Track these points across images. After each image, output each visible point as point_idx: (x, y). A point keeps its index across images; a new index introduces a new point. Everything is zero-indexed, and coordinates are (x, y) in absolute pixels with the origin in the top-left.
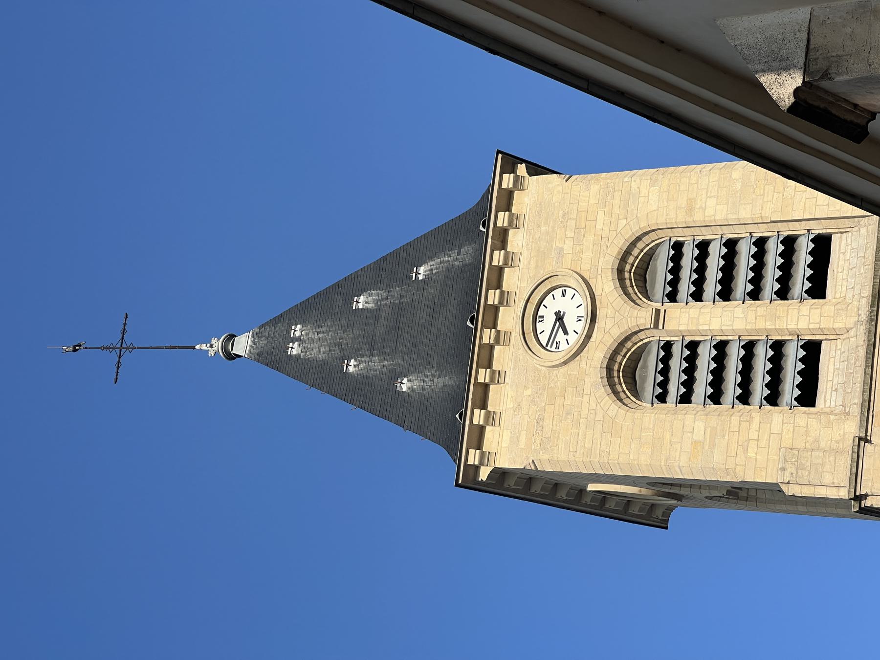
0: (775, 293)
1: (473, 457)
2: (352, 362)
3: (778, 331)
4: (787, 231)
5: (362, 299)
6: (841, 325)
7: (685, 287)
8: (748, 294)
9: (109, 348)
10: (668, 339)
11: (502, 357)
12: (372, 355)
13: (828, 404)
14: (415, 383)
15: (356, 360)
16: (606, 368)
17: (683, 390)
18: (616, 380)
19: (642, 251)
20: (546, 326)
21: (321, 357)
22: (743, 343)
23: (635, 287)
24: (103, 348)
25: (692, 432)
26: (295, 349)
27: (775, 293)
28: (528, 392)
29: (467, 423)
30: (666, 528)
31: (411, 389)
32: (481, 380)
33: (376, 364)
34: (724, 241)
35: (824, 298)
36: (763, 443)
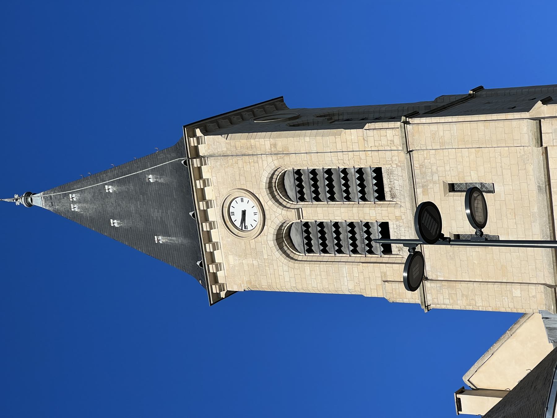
1: (215, 289)
10: (306, 221)
11: (215, 236)
16: (280, 249)
18: (274, 188)
19: (277, 179)
20: (237, 219)
23: (290, 248)
29: (198, 211)
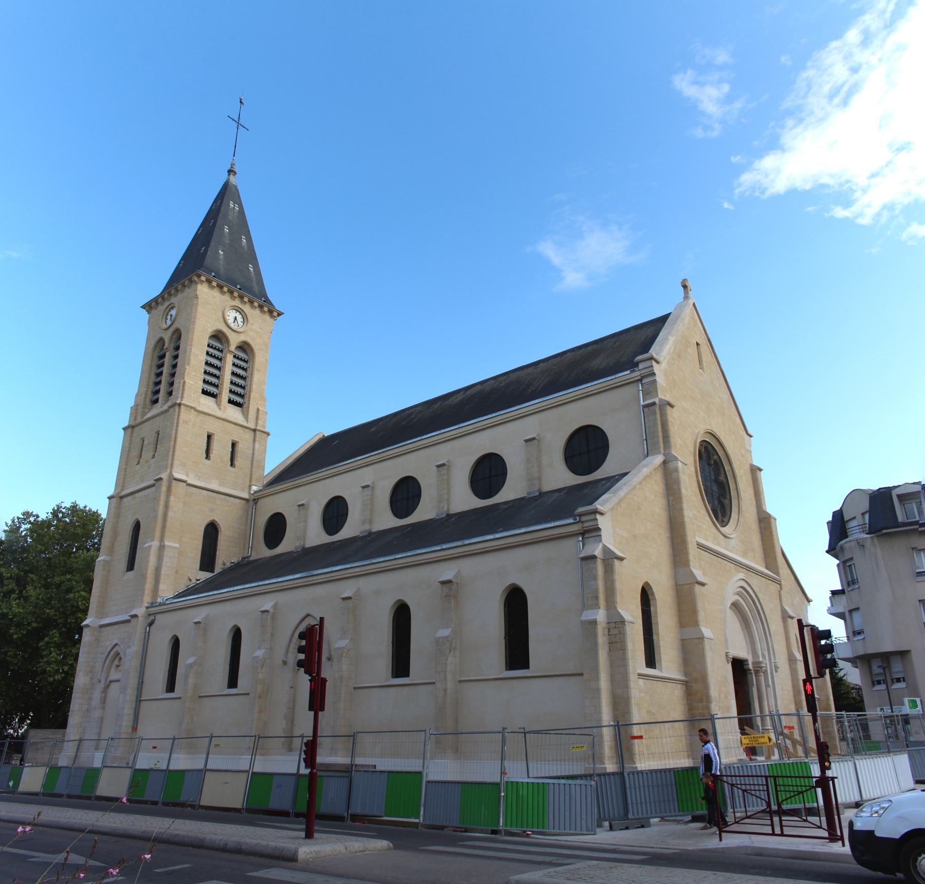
1: (203, 278)
2: (228, 231)
5: (245, 241)
24: (239, 115)
26: (232, 206)
28: (218, 303)
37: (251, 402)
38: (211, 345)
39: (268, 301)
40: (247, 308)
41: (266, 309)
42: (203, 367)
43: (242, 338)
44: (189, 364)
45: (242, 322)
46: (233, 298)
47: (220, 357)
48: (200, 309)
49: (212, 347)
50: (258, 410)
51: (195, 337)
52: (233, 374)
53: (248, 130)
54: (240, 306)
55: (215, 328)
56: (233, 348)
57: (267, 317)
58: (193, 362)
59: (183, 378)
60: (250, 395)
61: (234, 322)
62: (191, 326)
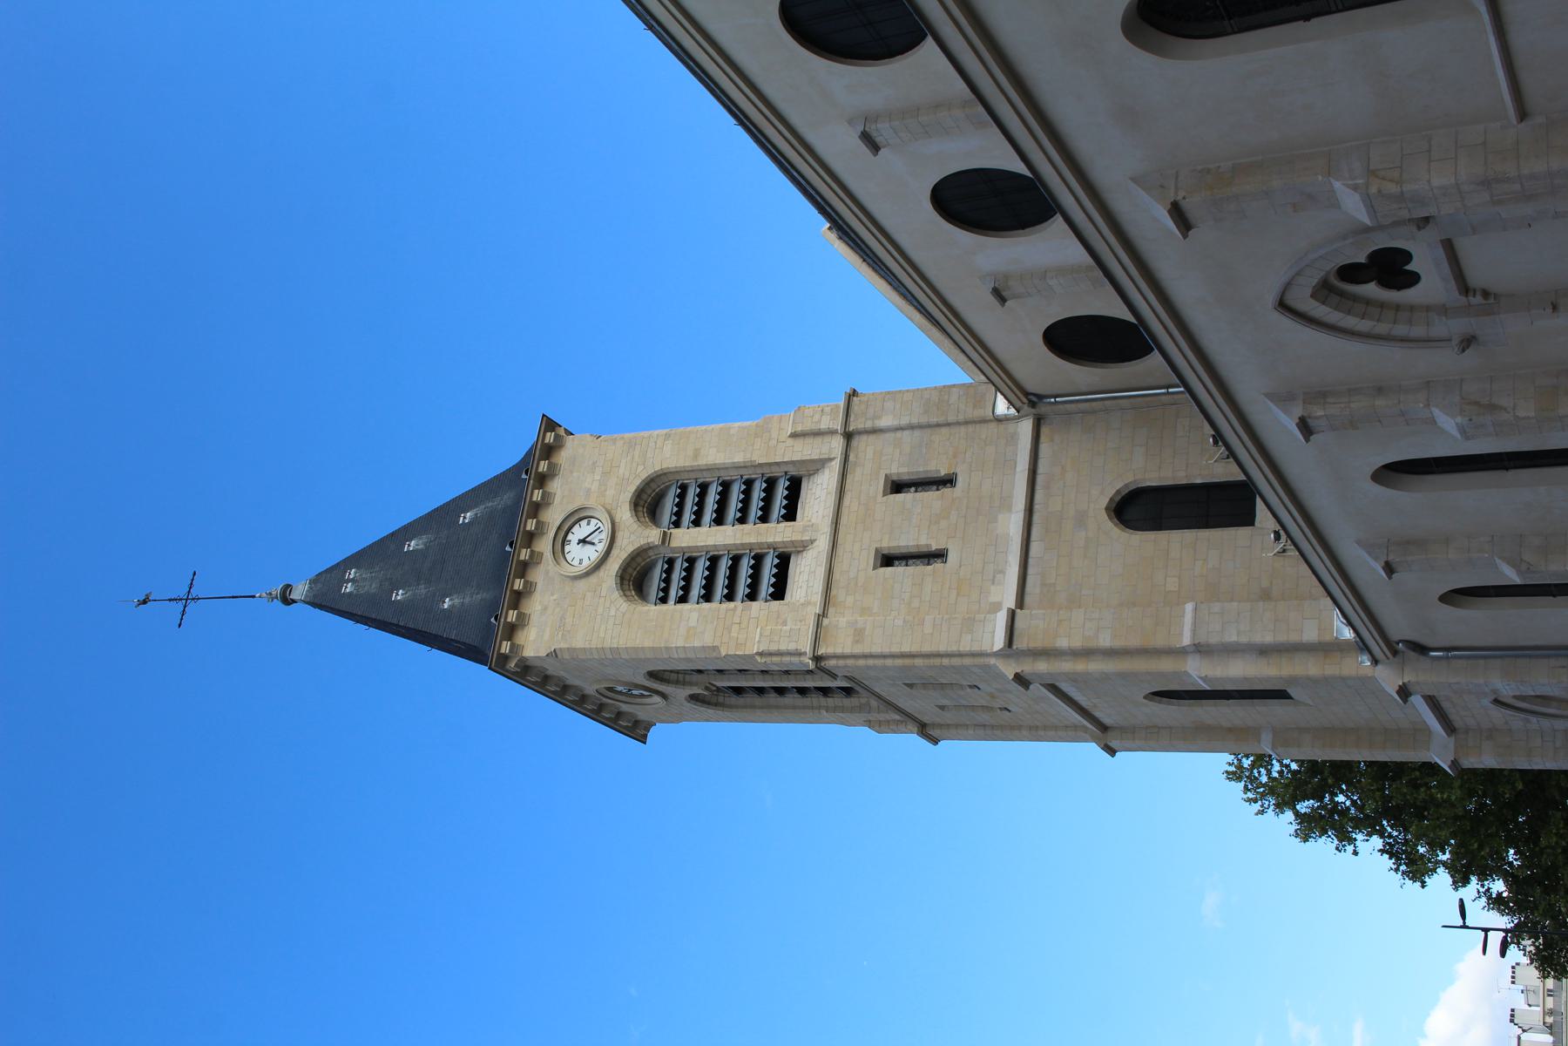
0: (770, 595)
1: (505, 647)
3: (760, 545)
4: (769, 473)
6: (808, 538)
7: (688, 516)
8: (737, 520)
9: (176, 600)
10: (671, 555)
12: (418, 585)
13: (794, 599)
14: (456, 601)
15: (403, 590)
17: (681, 593)
21: (373, 590)
22: (731, 556)
24: (170, 600)
25: (688, 621)
26: (349, 588)
27: (770, 595)
28: (555, 597)
30: (645, 743)
31: (452, 606)
32: (516, 587)
33: (422, 590)
34: (720, 482)
35: (795, 520)
36: (743, 626)
37: (778, 460)
38: (661, 594)
39: (525, 464)
40: (553, 517)
41: (543, 466)
42: (717, 607)
43: (625, 515)
44: (715, 648)
45: (588, 524)
46: (536, 559)
47: (686, 565)
48: (579, 642)
49: (666, 590)
50: (794, 435)
51: (648, 644)
52: (719, 520)
53: (195, 574)
54: (552, 534)
55: (616, 594)
56: (653, 535)
57: (563, 457)
58: (708, 640)
59: (751, 657)
60: (761, 465)
61: (593, 544)
62: (625, 656)
